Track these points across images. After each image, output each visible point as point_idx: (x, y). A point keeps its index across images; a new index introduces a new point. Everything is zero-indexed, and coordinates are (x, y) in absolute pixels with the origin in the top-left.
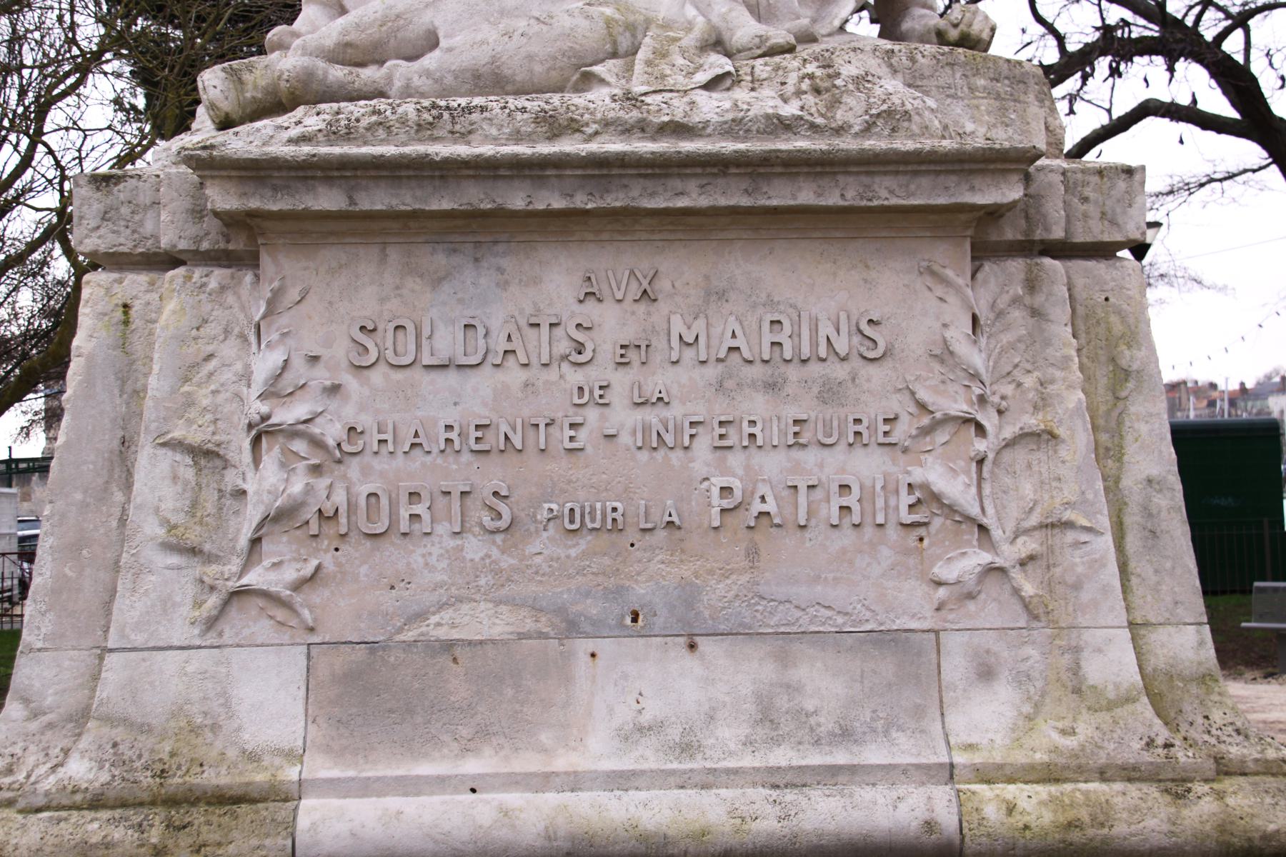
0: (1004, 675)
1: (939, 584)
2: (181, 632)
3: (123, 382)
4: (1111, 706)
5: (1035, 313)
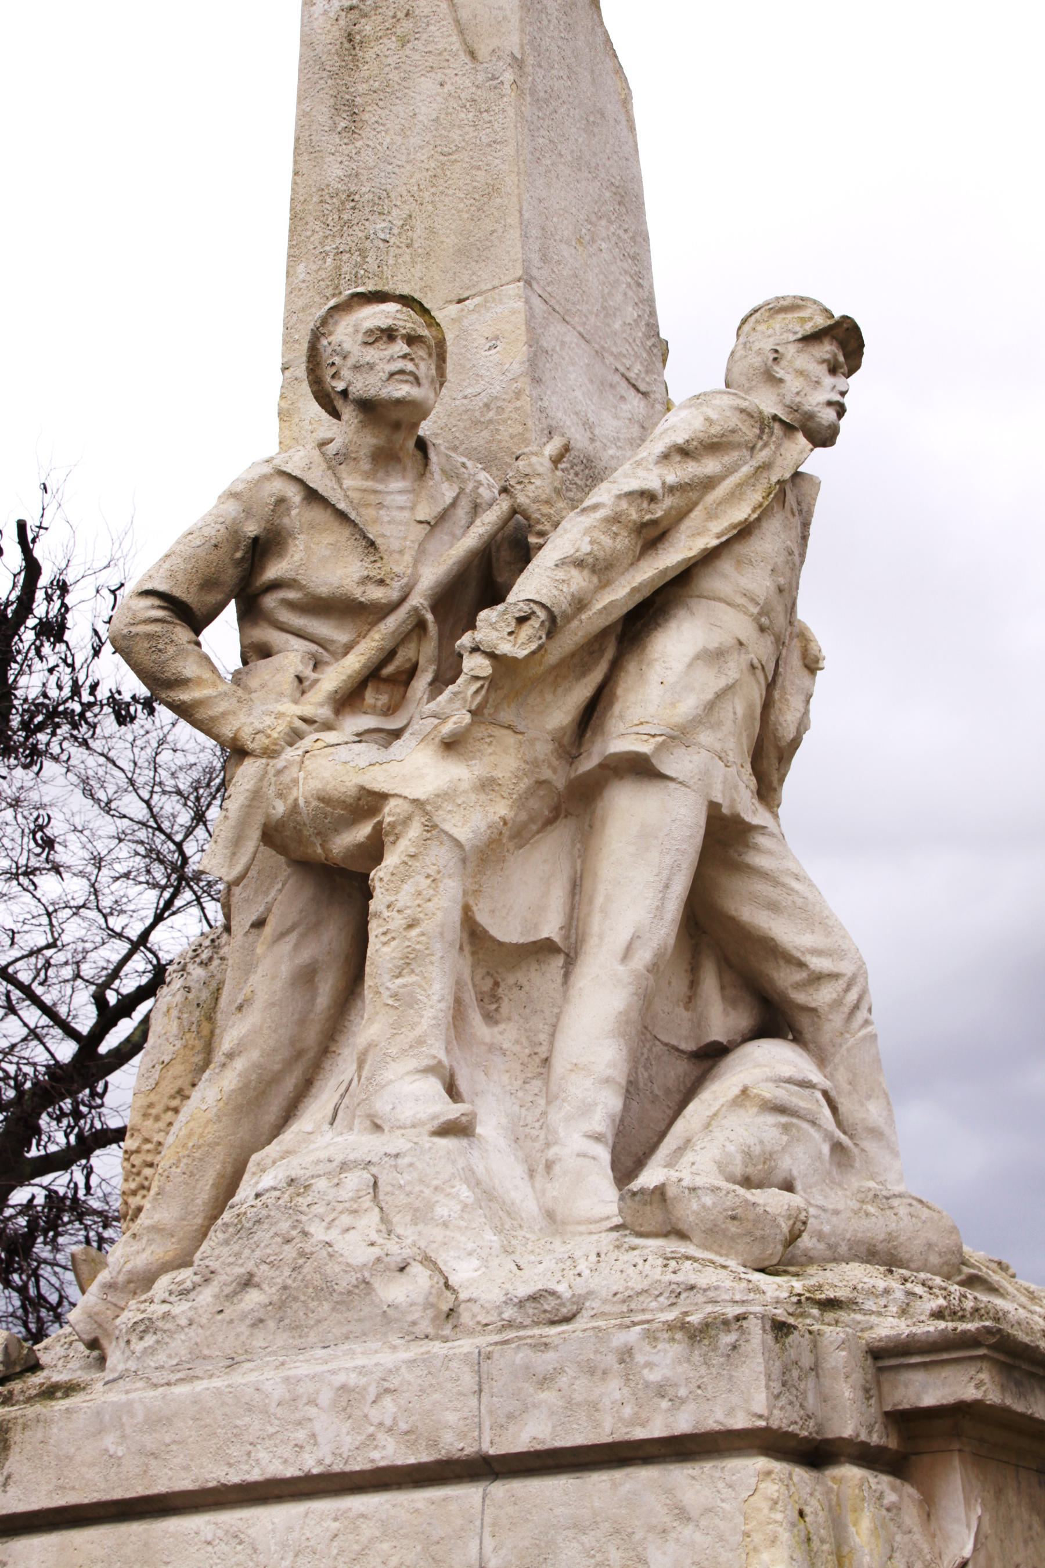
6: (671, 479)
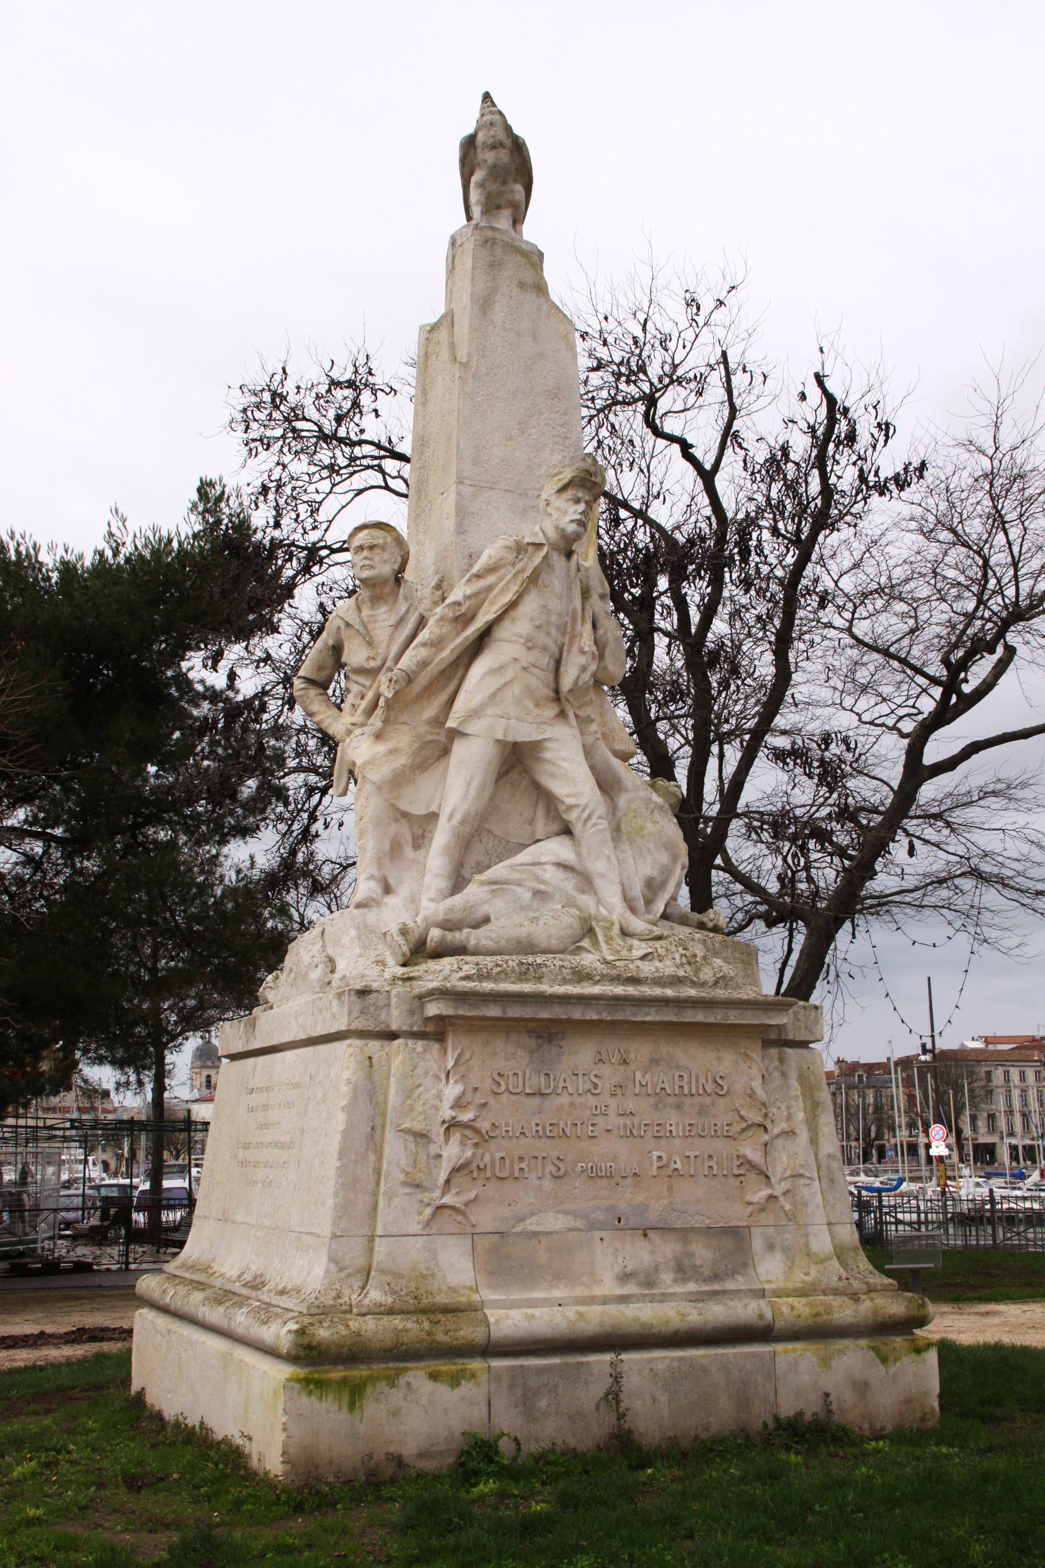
0: (778, 1248)
1: (750, 1204)
2: (415, 1228)
3: (371, 1098)
4: (822, 1261)
5: (783, 1074)
6: (469, 592)
